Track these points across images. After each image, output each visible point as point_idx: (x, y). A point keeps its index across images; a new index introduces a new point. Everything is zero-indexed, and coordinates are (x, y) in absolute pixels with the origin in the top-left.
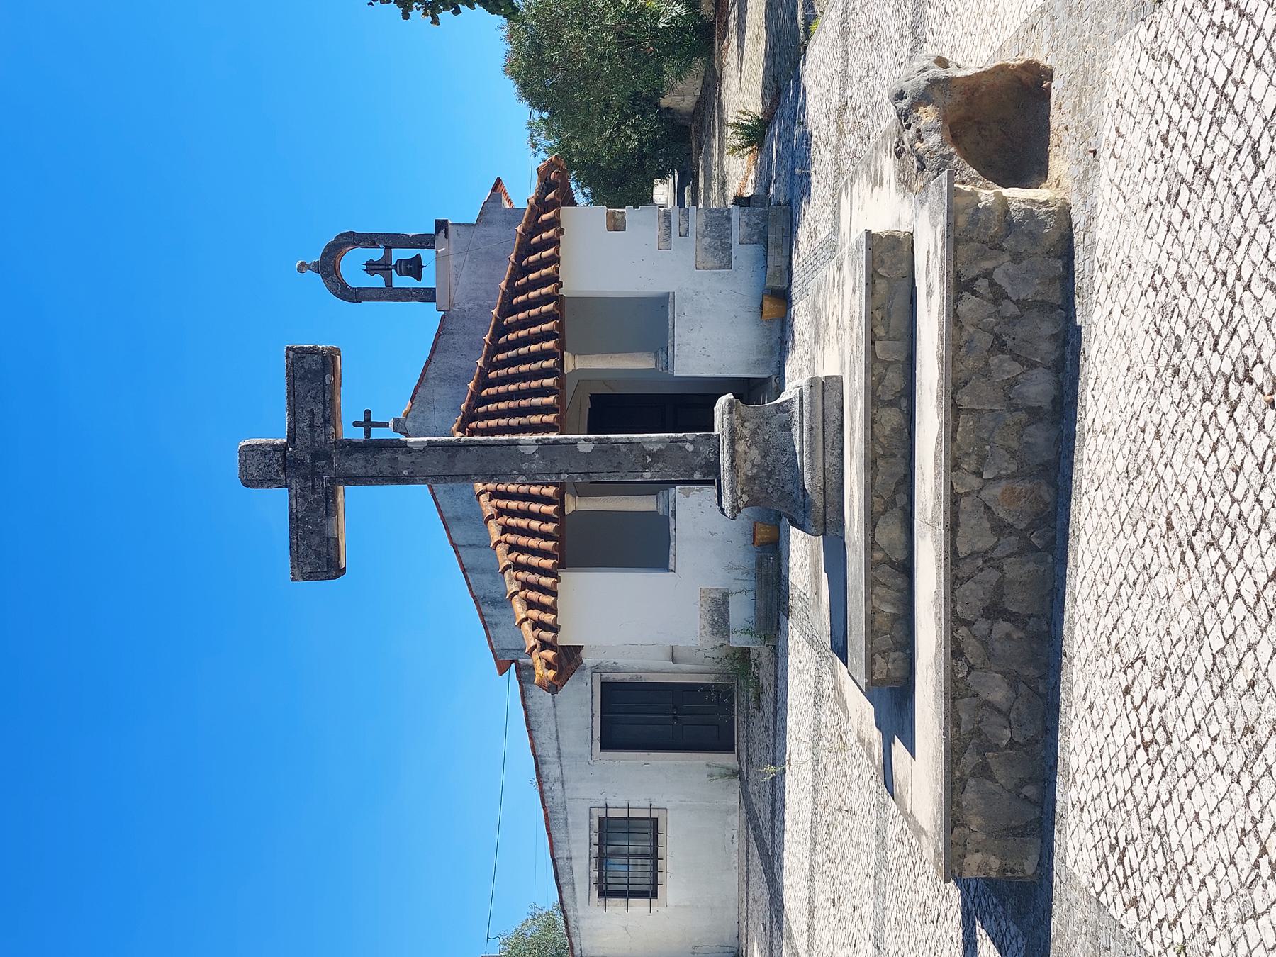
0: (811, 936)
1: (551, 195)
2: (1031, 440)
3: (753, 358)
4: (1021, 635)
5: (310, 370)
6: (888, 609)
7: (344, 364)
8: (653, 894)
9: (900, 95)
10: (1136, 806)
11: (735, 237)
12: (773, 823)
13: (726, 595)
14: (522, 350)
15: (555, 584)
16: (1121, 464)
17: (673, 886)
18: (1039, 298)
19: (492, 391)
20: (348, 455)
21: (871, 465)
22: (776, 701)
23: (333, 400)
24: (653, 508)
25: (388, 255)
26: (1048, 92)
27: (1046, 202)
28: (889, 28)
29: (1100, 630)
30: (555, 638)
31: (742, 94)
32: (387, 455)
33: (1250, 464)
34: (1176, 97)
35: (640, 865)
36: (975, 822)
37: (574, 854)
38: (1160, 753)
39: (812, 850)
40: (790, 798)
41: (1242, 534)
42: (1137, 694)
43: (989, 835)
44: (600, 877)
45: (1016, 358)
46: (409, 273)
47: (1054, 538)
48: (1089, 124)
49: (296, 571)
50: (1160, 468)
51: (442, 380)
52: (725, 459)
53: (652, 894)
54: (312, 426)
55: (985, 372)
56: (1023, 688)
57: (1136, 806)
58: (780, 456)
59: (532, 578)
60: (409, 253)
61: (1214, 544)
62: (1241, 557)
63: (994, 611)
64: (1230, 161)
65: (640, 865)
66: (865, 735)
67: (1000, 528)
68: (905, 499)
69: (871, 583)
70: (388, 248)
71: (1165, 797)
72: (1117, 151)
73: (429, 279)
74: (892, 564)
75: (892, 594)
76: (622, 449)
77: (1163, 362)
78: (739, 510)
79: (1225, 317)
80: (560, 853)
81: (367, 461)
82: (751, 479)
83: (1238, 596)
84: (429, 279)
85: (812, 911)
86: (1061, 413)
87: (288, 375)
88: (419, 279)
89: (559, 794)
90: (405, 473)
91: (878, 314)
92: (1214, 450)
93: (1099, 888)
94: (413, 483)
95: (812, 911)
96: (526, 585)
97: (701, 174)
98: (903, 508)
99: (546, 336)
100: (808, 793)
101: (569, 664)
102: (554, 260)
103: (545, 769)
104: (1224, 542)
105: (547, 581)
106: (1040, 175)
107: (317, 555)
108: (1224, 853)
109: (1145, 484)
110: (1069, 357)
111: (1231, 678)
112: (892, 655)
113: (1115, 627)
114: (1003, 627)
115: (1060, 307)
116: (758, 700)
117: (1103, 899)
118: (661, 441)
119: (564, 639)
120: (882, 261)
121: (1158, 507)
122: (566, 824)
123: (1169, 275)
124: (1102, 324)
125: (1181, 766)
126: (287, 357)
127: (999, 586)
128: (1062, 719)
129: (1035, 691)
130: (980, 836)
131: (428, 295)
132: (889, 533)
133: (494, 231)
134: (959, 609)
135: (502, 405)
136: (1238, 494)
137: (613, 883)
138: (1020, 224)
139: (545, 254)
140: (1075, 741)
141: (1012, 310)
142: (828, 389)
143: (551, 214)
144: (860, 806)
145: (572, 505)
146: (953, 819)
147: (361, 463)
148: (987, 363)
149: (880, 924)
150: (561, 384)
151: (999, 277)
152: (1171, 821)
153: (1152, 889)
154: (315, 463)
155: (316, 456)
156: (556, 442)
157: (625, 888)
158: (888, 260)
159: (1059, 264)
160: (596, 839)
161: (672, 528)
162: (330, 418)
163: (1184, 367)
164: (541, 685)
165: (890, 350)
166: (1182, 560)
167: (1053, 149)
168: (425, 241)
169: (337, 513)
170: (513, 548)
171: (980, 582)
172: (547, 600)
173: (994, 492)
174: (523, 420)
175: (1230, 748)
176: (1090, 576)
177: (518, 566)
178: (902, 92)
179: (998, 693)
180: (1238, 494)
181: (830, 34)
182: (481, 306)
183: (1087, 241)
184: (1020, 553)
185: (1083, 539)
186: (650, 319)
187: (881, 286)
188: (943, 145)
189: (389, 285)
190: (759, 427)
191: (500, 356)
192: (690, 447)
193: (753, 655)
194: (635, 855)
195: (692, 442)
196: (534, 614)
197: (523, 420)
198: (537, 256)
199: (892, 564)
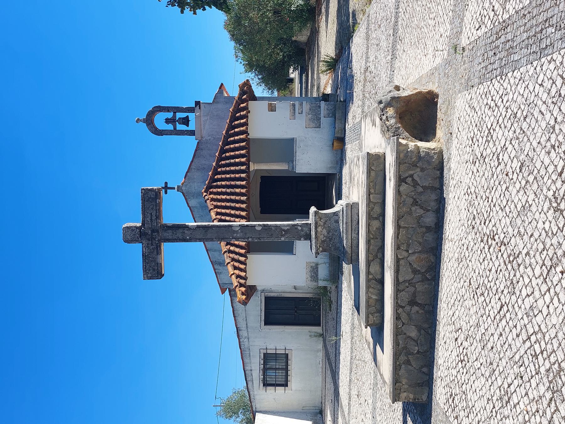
0: (349, 408)
1: (245, 97)
2: (427, 239)
3: (329, 166)
4: (422, 311)
6: (374, 297)
8: (286, 385)
9: (380, 102)
10: (458, 382)
11: (322, 115)
12: (336, 359)
13: (317, 265)
14: (232, 161)
15: (245, 260)
16: (456, 255)
18: (430, 185)
19: (219, 176)
20: (165, 231)
21: (368, 242)
22: (337, 309)
23: (159, 210)
25: (174, 116)
26: (437, 103)
27: (434, 149)
28: (384, 44)
29: (449, 315)
30: (245, 283)
31: (327, 47)
33: (494, 270)
34: (476, 125)
35: (281, 373)
36: (404, 381)
37: (253, 368)
38: (465, 365)
39: (350, 373)
40: (342, 350)
41: (491, 295)
42: (459, 341)
43: (410, 386)
45: (422, 208)
46: (183, 123)
47: (435, 275)
48: (450, 121)
49: (145, 276)
50: (468, 261)
51: (198, 170)
52: (313, 233)
54: (151, 219)
55: (410, 213)
56: (422, 332)
57: (458, 382)
59: (236, 257)
60: (184, 115)
61: (482, 294)
62: (490, 302)
63: (412, 303)
64: (491, 158)
65: (281, 373)
66: (367, 338)
67: (415, 271)
68: (381, 255)
69: (368, 287)
70: (175, 113)
71: (467, 381)
72: (458, 136)
73: (192, 126)
74: (376, 280)
75: (376, 291)
77: (469, 222)
78: (319, 254)
79: (488, 214)
80: (247, 368)
81: (173, 233)
83: (489, 316)
84: (192, 126)
85: (350, 398)
86: (438, 228)
87: (142, 200)
88: (188, 126)
89: (246, 343)
90: (188, 238)
91: (371, 184)
92: (484, 261)
93: (446, 410)
95: (350, 398)
96: (233, 260)
97: (310, 71)
99: (242, 156)
100: (349, 349)
101: (251, 291)
102: (246, 124)
103: (241, 333)
104: (486, 294)
105: (242, 259)
106: (433, 135)
107: (153, 269)
108: (483, 405)
109: (463, 265)
110: (441, 208)
111: (486, 344)
112: (376, 315)
113: (453, 315)
114: (415, 308)
115: (438, 189)
116: (330, 307)
117: (447, 414)
118: (288, 225)
119: (249, 283)
120: (373, 164)
121: (467, 275)
122: (250, 356)
123: (473, 191)
124: (452, 200)
125: (472, 371)
127: (414, 293)
128: (436, 344)
129: (427, 333)
130: (406, 386)
131: (192, 133)
132: (375, 268)
133: (220, 106)
134: (399, 302)
135: (223, 183)
136: (490, 279)
137: (269, 380)
138: (424, 157)
139: (242, 121)
140: (440, 354)
141: (420, 189)
142: (353, 207)
143: (244, 105)
144: (366, 368)
145: (253, 167)
146: (396, 380)
147: (171, 234)
148: (410, 209)
149: (375, 409)
150: (248, 176)
151: (415, 177)
152: (468, 390)
153: (462, 414)
154: (152, 235)
155: (153, 231)
156: (247, 226)
157: (274, 382)
158: (375, 163)
159: (438, 172)
160: (262, 362)
162: (159, 216)
163: (476, 228)
164: (239, 302)
165: (375, 198)
166: (474, 297)
167: (438, 125)
168: (190, 110)
169: (161, 253)
171: (407, 292)
172: (242, 266)
173: (412, 258)
174: (232, 190)
175: (486, 369)
176: (446, 294)
177: (230, 251)
178: (381, 101)
179: (413, 333)
180: (490, 279)
181: (362, 35)
182: (214, 138)
183: (448, 167)
184: (422, 281)
185: (444, 279)
186: (286, 148)
187: (373, 174)
188: (396, 123)
189: (175, 128)
190: (326, 221)
191: (223, 162)
192: (300, 228)
193: (329, 289)
194: (279, 369)
195: (300, 226)
196: (237, 272)
197: (232, 190)
198: (238, 122)
199: (376, 280)
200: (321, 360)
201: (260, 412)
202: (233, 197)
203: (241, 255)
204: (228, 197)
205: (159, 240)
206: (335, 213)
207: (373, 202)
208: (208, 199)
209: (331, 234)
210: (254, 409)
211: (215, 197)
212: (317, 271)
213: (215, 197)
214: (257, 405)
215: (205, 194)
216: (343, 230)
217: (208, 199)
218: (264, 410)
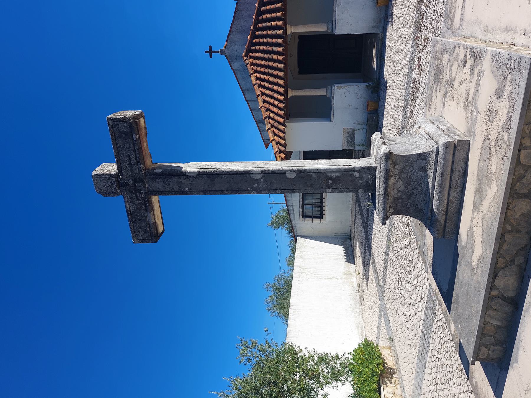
5: (123, 132)
13: (354, 131)
15: (284, 129)
17: (328, 215)
24: (325, 94)
32: (175, 180)
37: (294, 204)
44: (303, 211)
49: (135, 239)
51: (238, 32)
53: (321, 217)
54: (130, 164)
58: (417, 187)
59: (276, 124)
74: (503, 298)
76: (314, 176)
81: (165, 183)
82: (396, 199)
90: (187, 189)
94: (192, 194)
98: (519, 266)
112: (492, 347)
119: (288, 149)
126: (109, 124)
135: (261, 48)
145: (290, 94)
155: (135, 181)
160: (301, 200)
161: (332, 103)
162: (140, 160)
169: (153, 209)
170: (268, 110)
195: (358, 172)
199: (503, 298)
200: (351, 198)
201: (301, 236)
202: (271, 64)
203: (280, 123)
204: (266, 63)
205: (146, 193)
206: (420, 155)
207: (524, 165)
208: (248, 63)
209: (410, 188)
210: (296, 234)
211: (254, 61)
212: (354, 136)
213: (254, 61)
214: (298, 231)
215: (245, 58)
216: (433, 187)
217: (248, 63)
218: (303, 234)
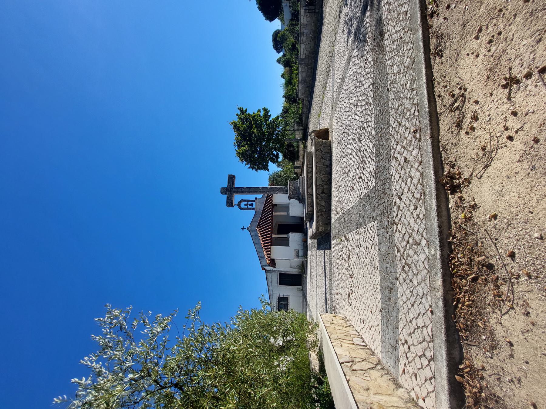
7: (236, 178)
63: (323, 193)
67: (323, 181)
73: (254, 206)
84: (254, 206)
114: (324, 195)
131: (253, 209)
132: (310, 190)
145: (273, 236)
162: (234, 184)
168: (253, 201)
179: (323, 204)
